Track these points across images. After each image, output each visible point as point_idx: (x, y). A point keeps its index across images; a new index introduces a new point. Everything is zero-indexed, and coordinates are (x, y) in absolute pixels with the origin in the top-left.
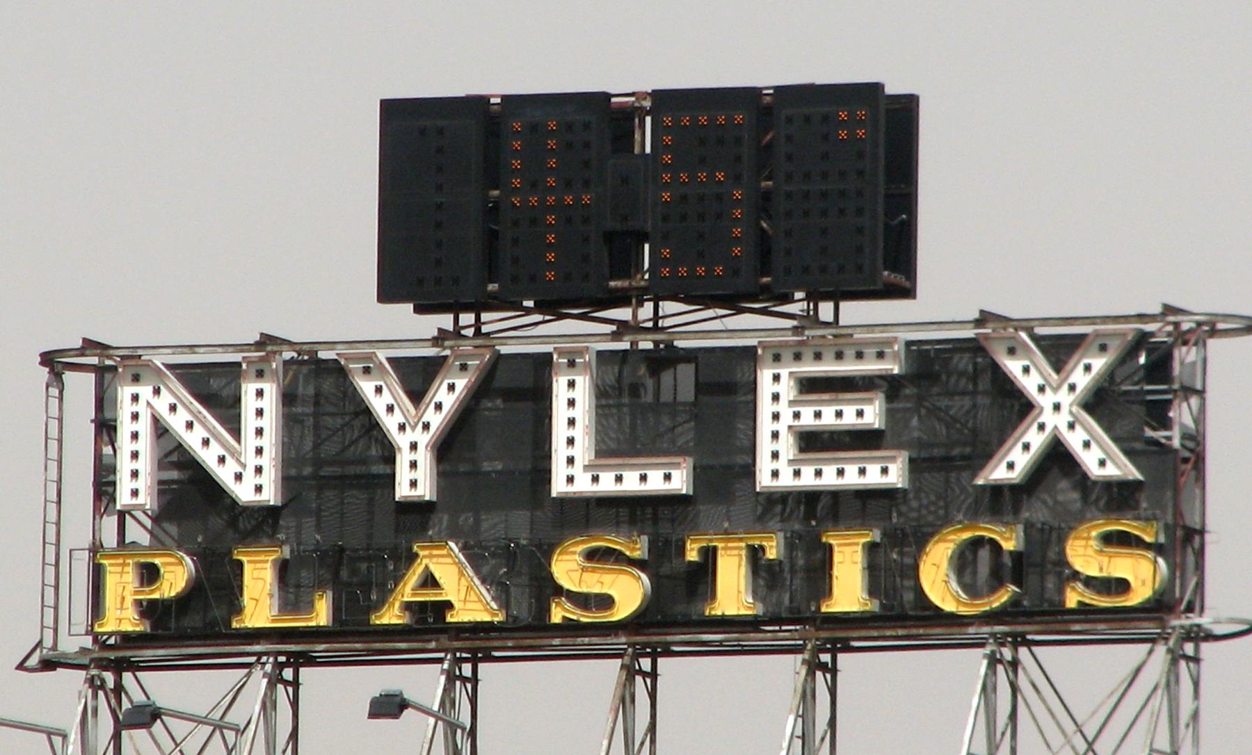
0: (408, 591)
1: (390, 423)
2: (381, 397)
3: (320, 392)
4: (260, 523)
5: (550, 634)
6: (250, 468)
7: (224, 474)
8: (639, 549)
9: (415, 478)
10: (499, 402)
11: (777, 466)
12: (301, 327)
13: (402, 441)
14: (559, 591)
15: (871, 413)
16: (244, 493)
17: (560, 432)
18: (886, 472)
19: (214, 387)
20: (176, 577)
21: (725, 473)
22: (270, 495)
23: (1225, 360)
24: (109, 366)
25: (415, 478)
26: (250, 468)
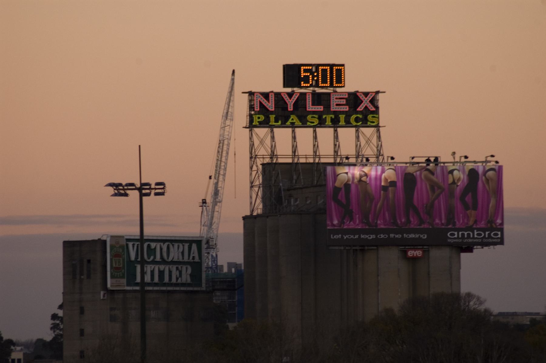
0: (290, 121)
1: (287, 101)
2: (286, 98)
3: (278, 95)
4: (272, 113)
5: (501, 205)
6: (271, 106)
7: (267, 107)
8: (317, 116)
9: (290, 108)
10: (464, 247)
11: (334, 108)
12: (276, 90)
13: (289, 103)
14: (308, 121)
15: (344, 102)
16: (270, 109)
17: (307, 101)
18: (346, 108)
19: (266, 95)
20: (262, 118)
21: (327, 107)
22: (273, 110)
23: (380, 97)
24: (251, 94)
25: (290, 108)
26: (271, 106)
